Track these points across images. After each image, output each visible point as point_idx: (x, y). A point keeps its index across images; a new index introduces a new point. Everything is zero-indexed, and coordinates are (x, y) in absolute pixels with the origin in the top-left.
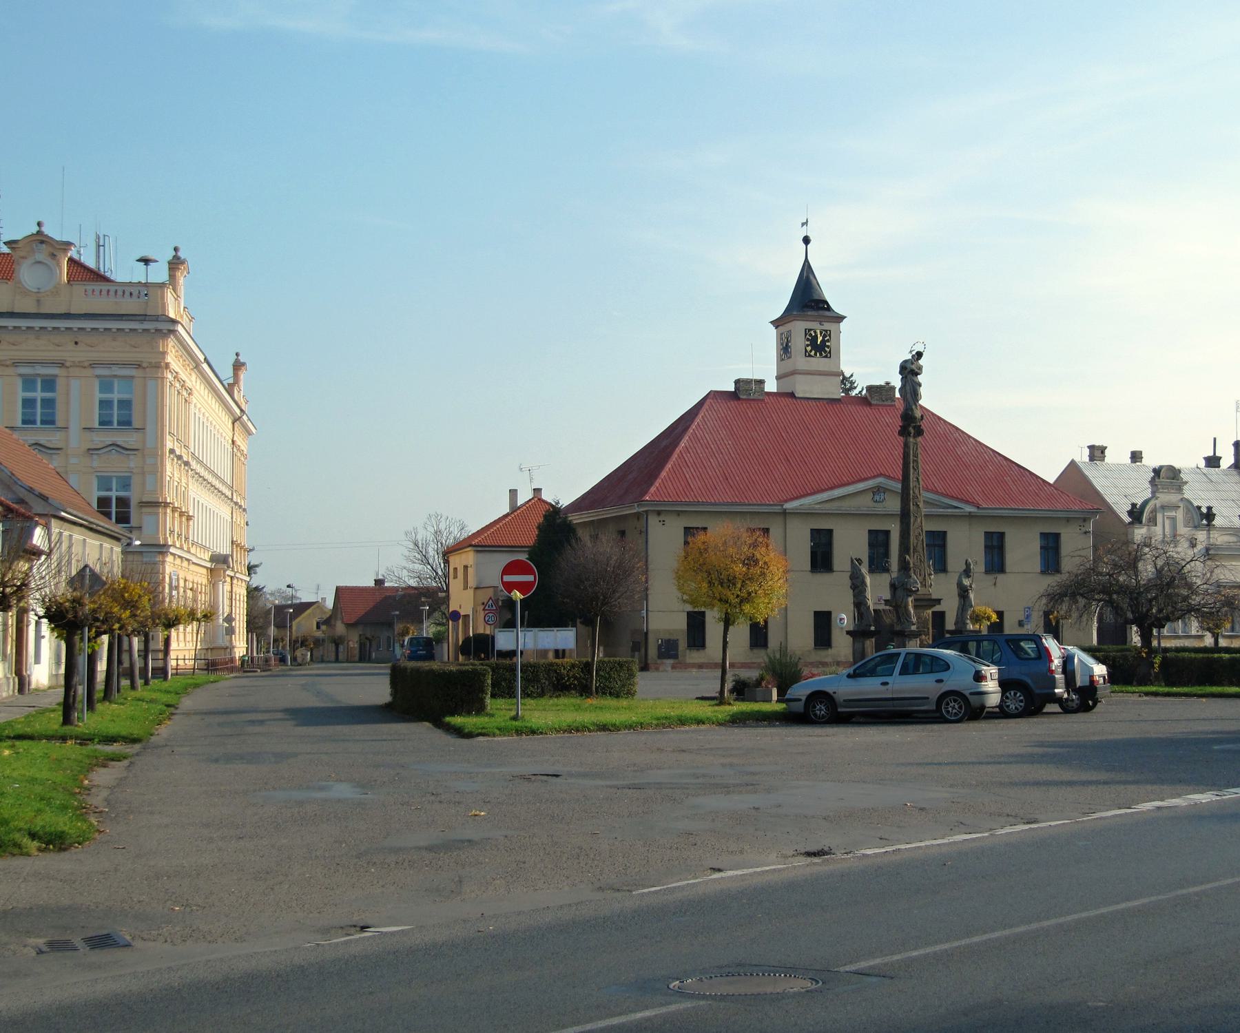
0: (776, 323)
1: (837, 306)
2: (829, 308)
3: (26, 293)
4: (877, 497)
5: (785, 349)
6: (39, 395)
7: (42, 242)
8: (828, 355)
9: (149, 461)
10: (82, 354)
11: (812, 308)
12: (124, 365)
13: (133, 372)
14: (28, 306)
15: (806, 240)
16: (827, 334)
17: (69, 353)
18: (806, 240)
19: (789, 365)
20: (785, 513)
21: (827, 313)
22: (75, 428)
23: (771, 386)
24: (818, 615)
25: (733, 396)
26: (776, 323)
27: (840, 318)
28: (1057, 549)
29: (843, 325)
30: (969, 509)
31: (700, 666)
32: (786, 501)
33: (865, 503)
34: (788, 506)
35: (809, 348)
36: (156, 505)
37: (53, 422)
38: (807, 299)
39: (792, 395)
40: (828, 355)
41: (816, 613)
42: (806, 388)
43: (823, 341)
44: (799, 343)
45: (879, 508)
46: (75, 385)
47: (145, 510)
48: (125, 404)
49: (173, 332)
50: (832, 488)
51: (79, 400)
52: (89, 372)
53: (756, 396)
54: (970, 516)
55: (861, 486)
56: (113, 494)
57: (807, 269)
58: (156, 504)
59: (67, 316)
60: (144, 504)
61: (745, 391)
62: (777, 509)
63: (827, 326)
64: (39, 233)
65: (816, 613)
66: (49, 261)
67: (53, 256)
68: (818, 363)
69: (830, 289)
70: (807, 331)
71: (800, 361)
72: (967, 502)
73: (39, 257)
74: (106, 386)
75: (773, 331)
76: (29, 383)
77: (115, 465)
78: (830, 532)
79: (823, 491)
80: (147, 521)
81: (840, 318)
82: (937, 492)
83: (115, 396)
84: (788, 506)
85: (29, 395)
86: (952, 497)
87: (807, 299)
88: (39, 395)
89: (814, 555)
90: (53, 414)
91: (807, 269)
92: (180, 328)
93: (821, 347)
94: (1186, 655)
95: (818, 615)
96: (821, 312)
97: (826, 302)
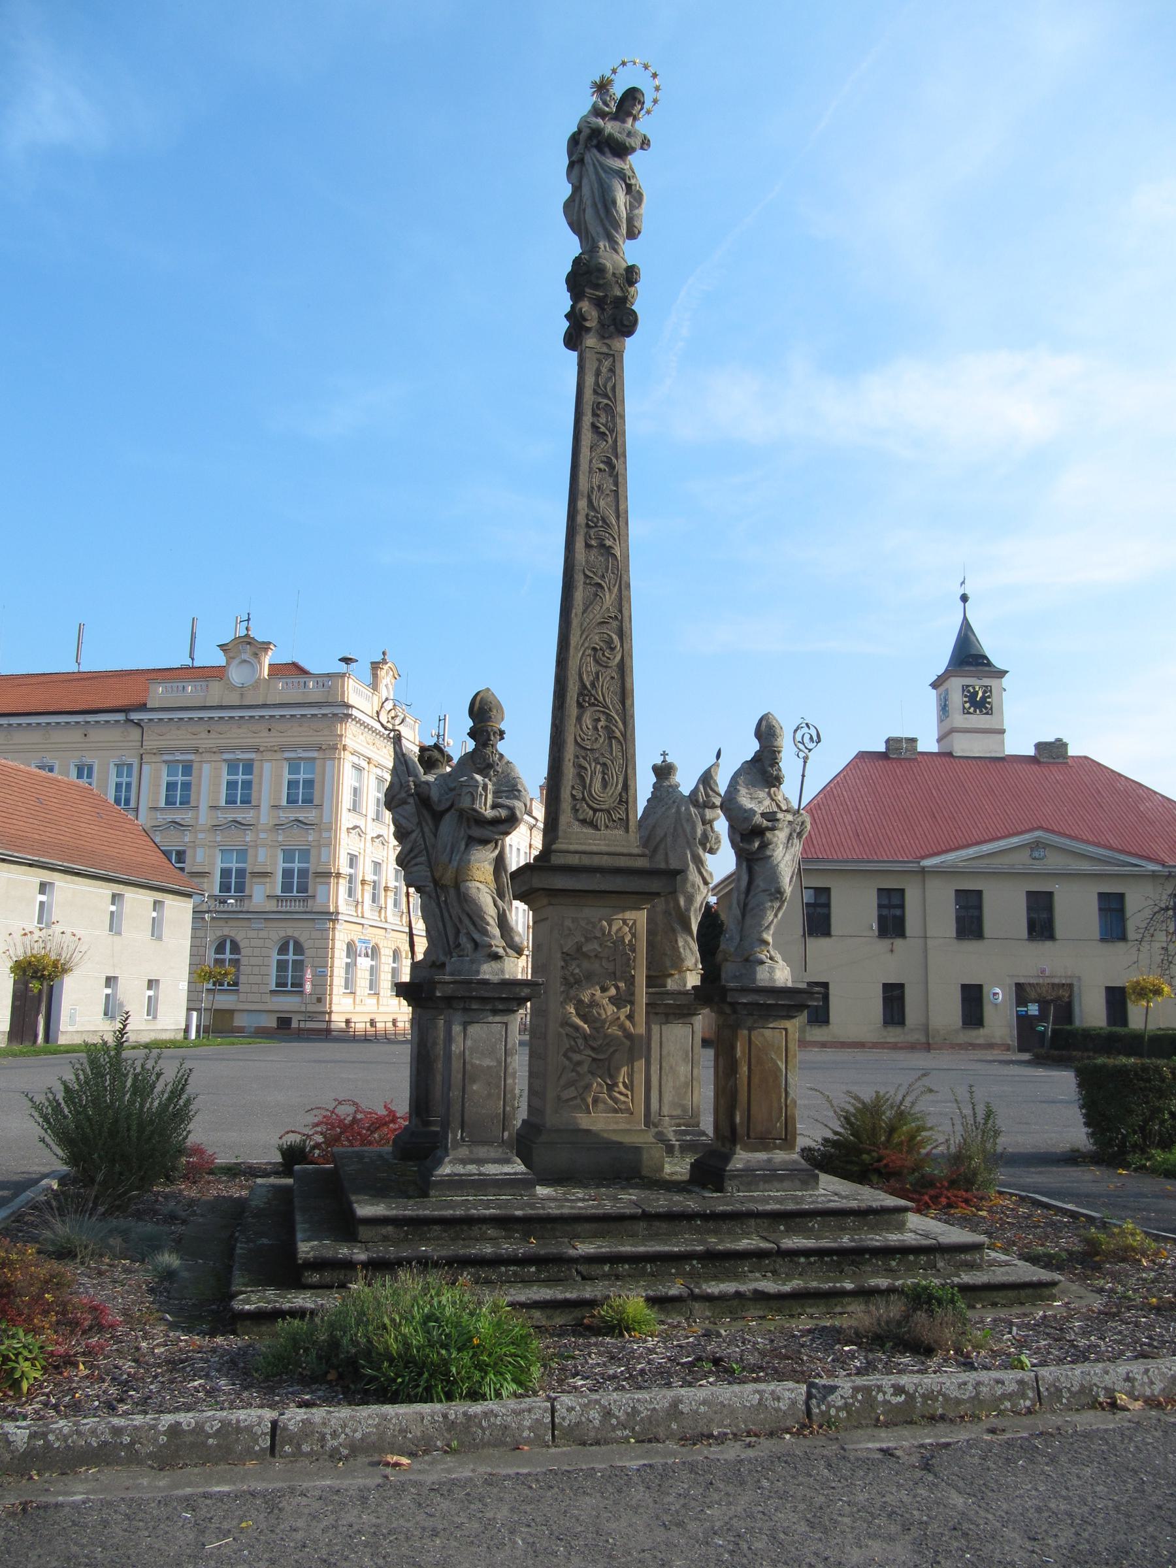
0: (935, 685)
1: (998, 662)
2: (989, 664)
3: (231, 687)
4: (1036, 854)
5: (944, 708)
6: (180, 778)
7: (249, 643)
8: (989, 712)
9: (325, 835)
10: (274, 740)
11: (969, 664)
12: (306, 748)
13: (315, 754)
14: (234, 699)
15: (964, 598)
16: (987, 689)
17: (265, 739)
18: (964, 598)
19: (947, 725)
20: (923, 872)
21: (987, 668)
22: (203, 807)
23: (928, 743)
24: (887, 987)
25: (883, 756)
26: (935, 685)
27: (1002, 673)
28: (1121, 910)
29: (1005, 681)
30: (1152, 867)
31: (824, 1045)
32: (923, 858)
33: (1021, 860)
34: (926, 863)
35: (967, 705)
36: (326, 875)
37: (249, 802)
38: (968, 657)
39: (950, 754)
40: (989, 712)
41: (885, 985)
42: (964, 746)
43: (984, 698)
44: (957, 699)
45: (1038, 867)
46: (267, 766)
47: (318, 880)
48: (309, 784)
49: (349, 716)
50: (977, 843)
51: (272, 781)
52: (279, 756)
53: (908, 755)
54: (1154, 876)
55: (1015, 841)
56: (296, 865)
57: (966, 627)
58: (328, 875)
59: (264, 706)
60: (319, 875)
61: (898, 752)
62: (912, 866)
63: (986, 682)
64: (247, 636)
65: (885, 985)
66: (253, 660)
67: (256, 655)
68: (978, 720)
69: (990, 645)
70: (965, 688)
71: (959, 720)
72: (1149, 859)
73: (244, 656)
74: (294, 769)
75: (933, 693)
76: (232, 767)
77: (297, 838)
78: (980, 893)
79: (968, 846)
80: (321, 889)
81: (1002, 673)
82: (1111, 848)
83: (302, 777)
84: (926, 863)
85: (119, 780)
86: (1129, 854)
87: (968, 657)
88: (240, 778)
89: (960, 920)
90: (312, 794)
91: (966, 627)
92: (355, 712)
93: (980, 703)
94: (721, 1070)
95: (887, 987)
96: (980, 668)
97: (986, 657)
